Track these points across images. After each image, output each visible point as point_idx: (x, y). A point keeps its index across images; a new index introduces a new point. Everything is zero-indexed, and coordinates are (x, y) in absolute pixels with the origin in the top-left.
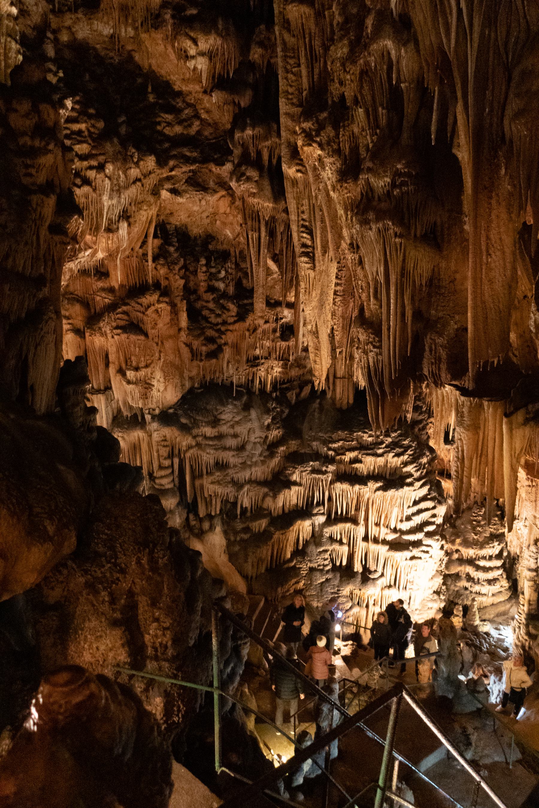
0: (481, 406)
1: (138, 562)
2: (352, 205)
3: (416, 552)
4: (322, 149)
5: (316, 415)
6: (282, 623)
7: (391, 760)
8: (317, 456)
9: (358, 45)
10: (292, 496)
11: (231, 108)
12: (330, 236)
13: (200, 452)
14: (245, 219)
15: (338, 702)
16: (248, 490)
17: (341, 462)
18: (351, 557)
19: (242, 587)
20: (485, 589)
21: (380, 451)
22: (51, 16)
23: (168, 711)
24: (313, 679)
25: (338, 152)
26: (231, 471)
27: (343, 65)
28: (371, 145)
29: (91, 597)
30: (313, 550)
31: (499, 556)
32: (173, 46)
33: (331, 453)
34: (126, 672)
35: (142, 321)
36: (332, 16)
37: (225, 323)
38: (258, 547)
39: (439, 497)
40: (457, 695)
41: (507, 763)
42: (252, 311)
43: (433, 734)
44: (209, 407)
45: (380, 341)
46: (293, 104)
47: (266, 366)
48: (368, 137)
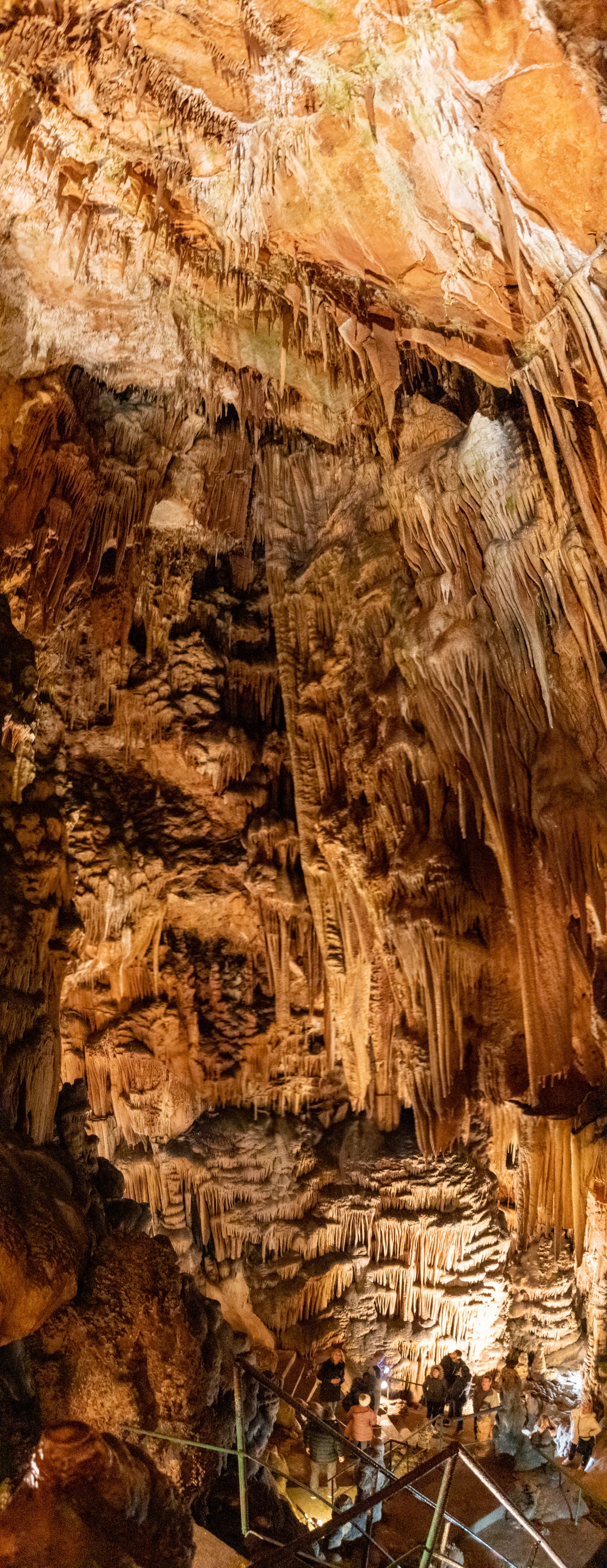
0: (546, 1125)
1: (147, 1312)
2: (383, 902)
3: (476, 1296)
5: (355, 1139)
6: (318, 1381)
7: (442, 1522)
8: (357, 1188)
9: (373, 748)
10: (327, 1237)
12: (361, 936)
13: (216, 1186)
14: (262, 920)
15: (383, 1465)
16: (275, 1230)
17: (386, 1194)
18: (400, 1305)
19: (269, 1341)
20: (553, 1332)
21: (432, 1180)
23: (185, 1475)
24: (354, 1441)
25: (363, 848)
26: (253, 1209)
27: (360, 765)
29: (93, 1348)
30: (353, 1297)
31: (568, 1295)
33: (374, 1184)
34: (136, 1431)
35: (147, 1037)
36: (345, 723)
37: (242, 1036)
38: (288, 1295)
39: (503, 1231)
40: (520, 1451)
41: (573, 1520)
42: (274, 1021)
43: (491, 1494)
44: (226, 1134)
45: (427, 1054)
47: (292, 1084)
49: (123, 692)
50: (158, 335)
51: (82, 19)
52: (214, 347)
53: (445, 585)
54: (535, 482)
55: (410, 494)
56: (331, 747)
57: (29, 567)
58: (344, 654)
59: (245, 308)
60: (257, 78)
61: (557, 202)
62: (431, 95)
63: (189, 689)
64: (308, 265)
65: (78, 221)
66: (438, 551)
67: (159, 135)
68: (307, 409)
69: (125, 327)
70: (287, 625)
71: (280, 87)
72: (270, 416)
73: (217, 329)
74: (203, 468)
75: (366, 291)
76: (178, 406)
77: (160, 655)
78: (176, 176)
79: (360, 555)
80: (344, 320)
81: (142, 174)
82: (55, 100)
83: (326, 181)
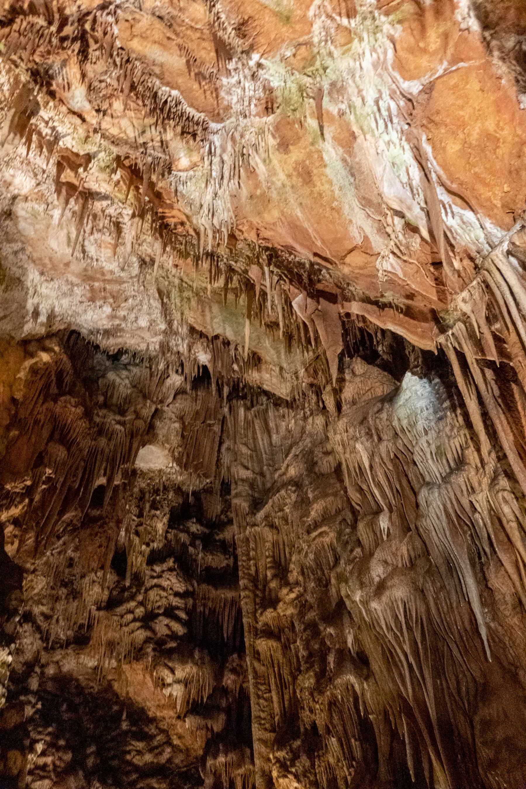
4: (299, 781)
9: (323, 678)
11: (204, 732)
22: (43, 653)
27: (311, 694)
28: (349, 778)
32: (152, 675)
46: (266, 729)
48: (345, 769)
49: (102, 613)
50: (145, 307)
51: (71, 19)
52: (192, 317)
53: (384, 522)
54: (462, 432)
55: (352, 442)
56: (285, 672)
57: (27, 500)
58: (297, 583)
59: (216, 285)
60: (225, 80)
61: (478, 186)
62: (371, 95)
63: (161, 611)
64: (267, 249)
65: (74, 205)
66: (376, 492)
67: (144, 132)
68: (267, 369)
69: (117, 299)
70: (248, 555)
71: (244, 89)
72: (236, 376)
73: (193, 303)
74: (181, 419)
75: (314, 271)
76: (161, 366)
77: (138, 579)
78: (159, 170)
79: (310, 495)
80: (296, 296)
81: (130, 167)
82: (52, 94)
83: (282, 176)
